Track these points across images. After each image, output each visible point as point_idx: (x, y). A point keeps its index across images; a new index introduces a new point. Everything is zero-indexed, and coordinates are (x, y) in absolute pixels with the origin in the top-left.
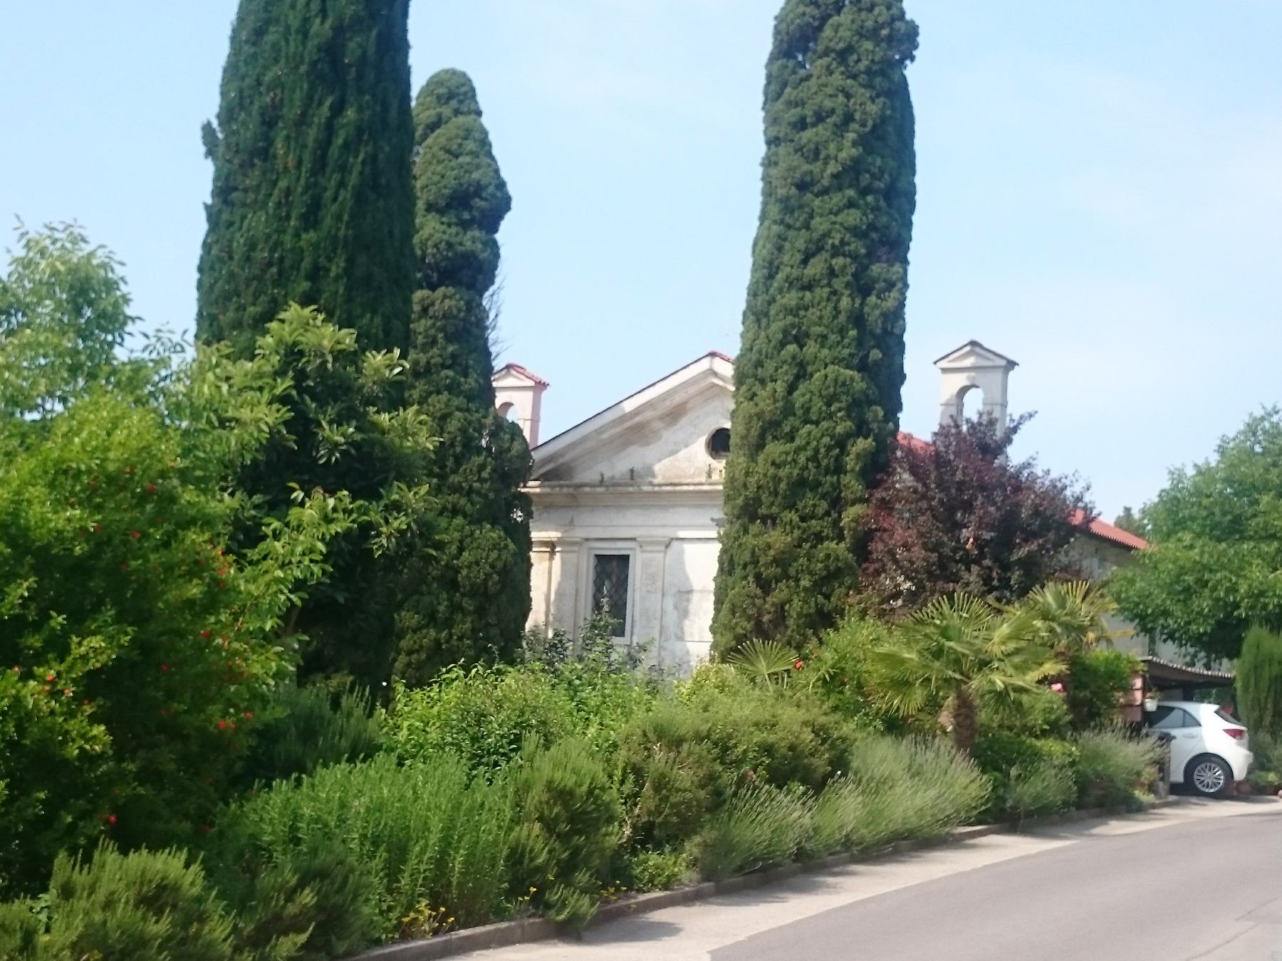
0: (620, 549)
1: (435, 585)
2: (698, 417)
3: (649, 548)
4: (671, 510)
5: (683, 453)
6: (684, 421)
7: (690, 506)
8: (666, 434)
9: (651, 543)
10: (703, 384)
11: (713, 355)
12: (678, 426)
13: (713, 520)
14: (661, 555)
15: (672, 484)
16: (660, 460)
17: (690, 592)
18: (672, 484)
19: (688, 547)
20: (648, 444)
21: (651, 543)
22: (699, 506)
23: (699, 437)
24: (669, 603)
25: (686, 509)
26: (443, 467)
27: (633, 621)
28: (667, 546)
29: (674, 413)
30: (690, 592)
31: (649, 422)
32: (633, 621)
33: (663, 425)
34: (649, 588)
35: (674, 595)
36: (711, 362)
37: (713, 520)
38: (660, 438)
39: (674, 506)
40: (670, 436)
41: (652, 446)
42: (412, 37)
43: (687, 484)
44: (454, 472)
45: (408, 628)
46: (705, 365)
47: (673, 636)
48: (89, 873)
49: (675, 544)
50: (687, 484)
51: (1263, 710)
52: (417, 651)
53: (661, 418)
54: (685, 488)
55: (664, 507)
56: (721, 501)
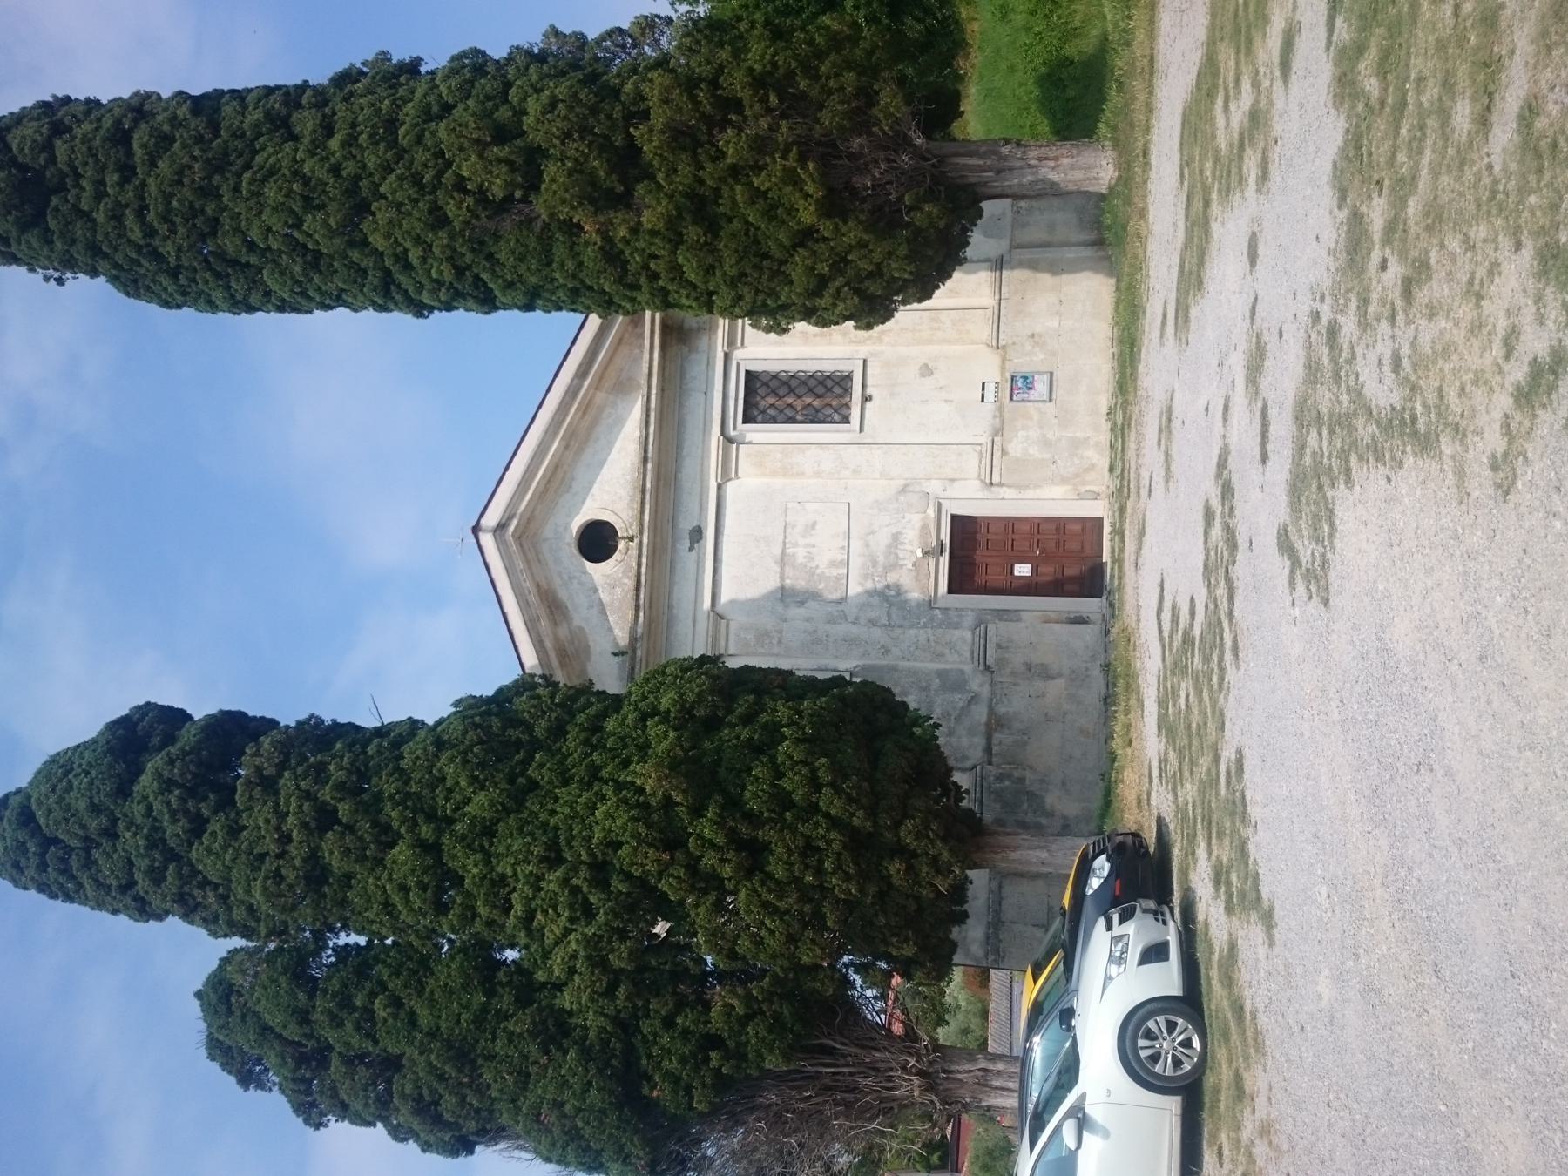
1: (707, 744)
2: (560, 574)
4: (675, 611)
5: (604, 596)
6: (562, 594)
8: (577, 621)
10: (514, 548)
11: (476, 529)
13: (691, 550)
16: (610, 630)
17: (783, 588)
18: (637, 589)
19: (725, 596)
23: (585, 573)
24: (795, 612)
26: (518, 745)
30: (783, 588)
31: (557, 639)
33: (565, 625)
34: (775, 642)
35: (787, 607)
36: (486, 531)
37: (691, 550)
38: (581, 629)
39: (670, 607)
40: (581, 616)
41: (591, 644)
43: (639, 565)
44: (529, 728)
45: (773, 785)
46: (487, 540)
49: (719, 609)
50: (639, 565)
52: (814, 771)
53: (555, 624)
54: (643, 570)
55: (671, 621)
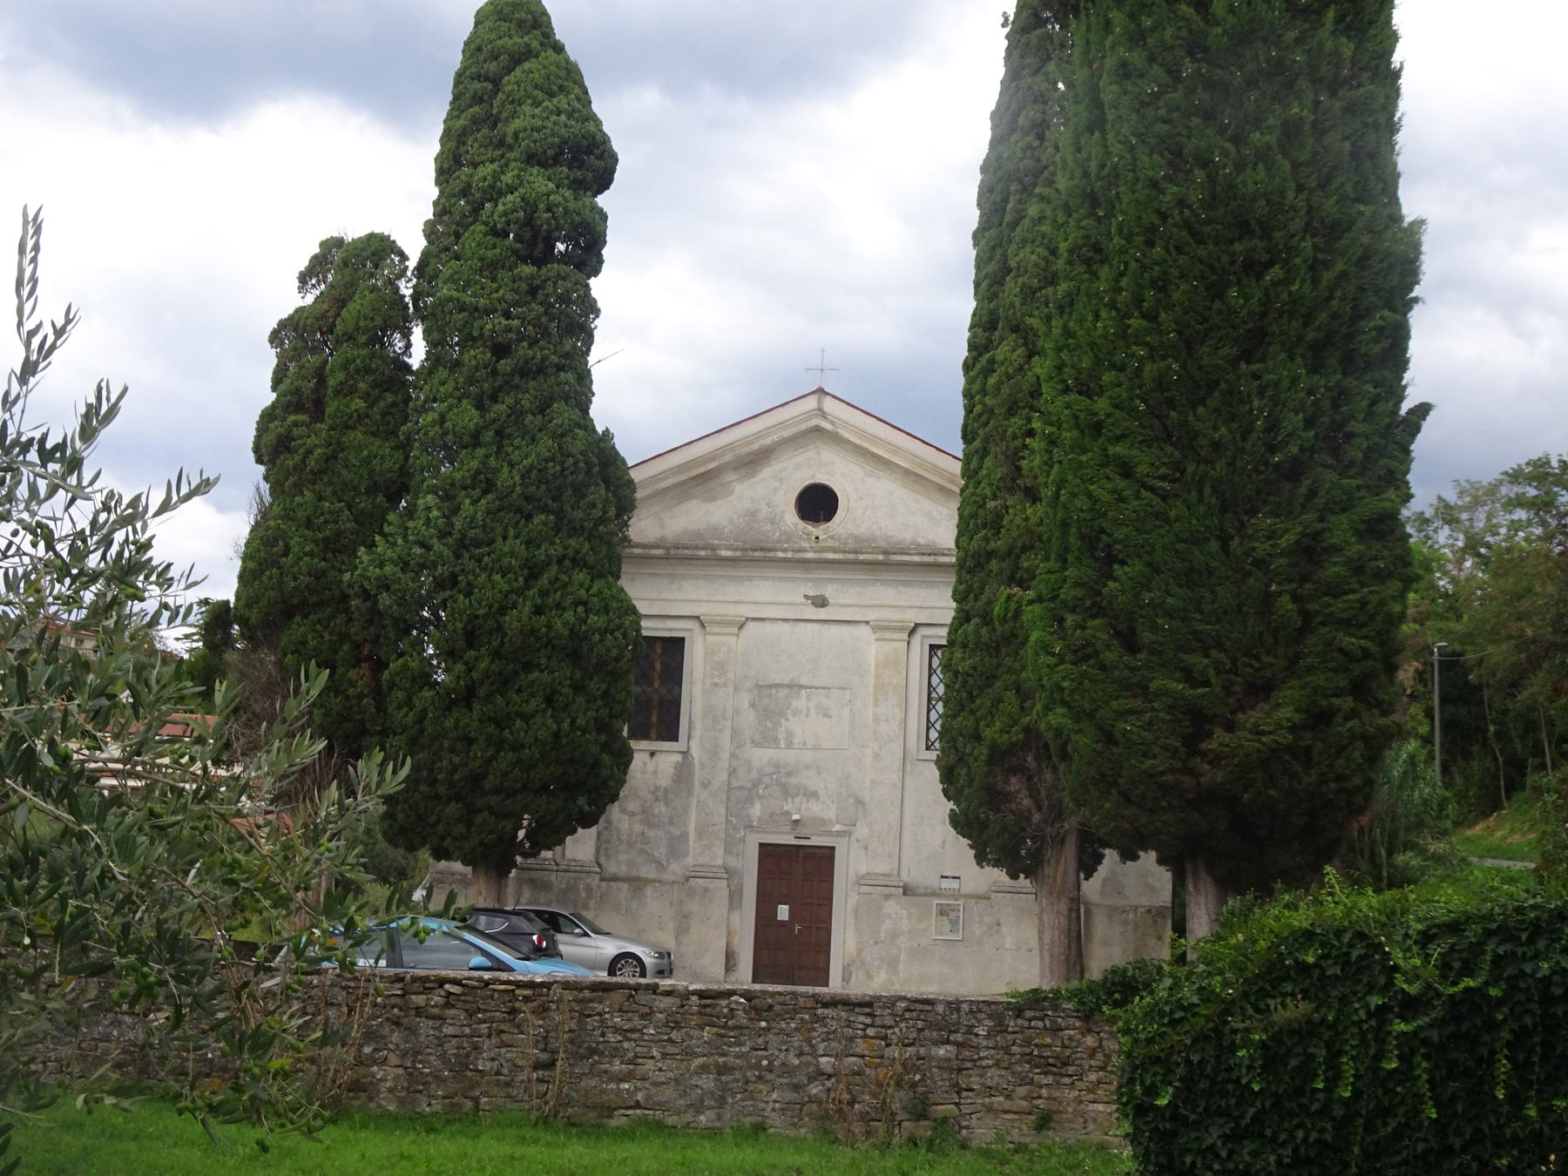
0: (670, 630)
3: (716, 630)
7: (773, 579)
9: (720, 623)
12: (756, 479)
13: (806, 597)
14: (733, 639)
15: (762, 549)
20: (714, 499)
21: (720, 623)
22: (788, 580)
25: (769, 583)
27: (690, 722)
28: (741, 628)
29: (753, 460)
32: (690, 722)
37: (806, 597)
41: (717, 503)
42: (998, 88)
47: (748, 743)
48: (457, 928)
51: (1013, 997)
56: (954, 570)
